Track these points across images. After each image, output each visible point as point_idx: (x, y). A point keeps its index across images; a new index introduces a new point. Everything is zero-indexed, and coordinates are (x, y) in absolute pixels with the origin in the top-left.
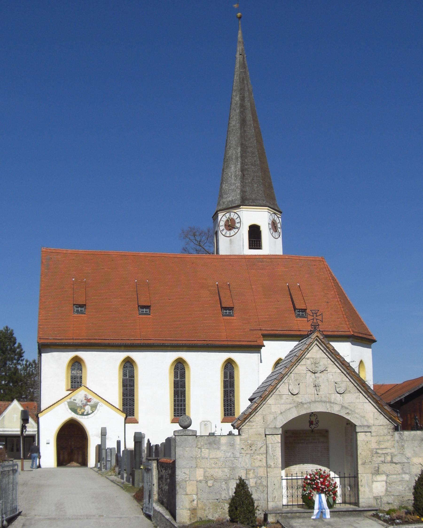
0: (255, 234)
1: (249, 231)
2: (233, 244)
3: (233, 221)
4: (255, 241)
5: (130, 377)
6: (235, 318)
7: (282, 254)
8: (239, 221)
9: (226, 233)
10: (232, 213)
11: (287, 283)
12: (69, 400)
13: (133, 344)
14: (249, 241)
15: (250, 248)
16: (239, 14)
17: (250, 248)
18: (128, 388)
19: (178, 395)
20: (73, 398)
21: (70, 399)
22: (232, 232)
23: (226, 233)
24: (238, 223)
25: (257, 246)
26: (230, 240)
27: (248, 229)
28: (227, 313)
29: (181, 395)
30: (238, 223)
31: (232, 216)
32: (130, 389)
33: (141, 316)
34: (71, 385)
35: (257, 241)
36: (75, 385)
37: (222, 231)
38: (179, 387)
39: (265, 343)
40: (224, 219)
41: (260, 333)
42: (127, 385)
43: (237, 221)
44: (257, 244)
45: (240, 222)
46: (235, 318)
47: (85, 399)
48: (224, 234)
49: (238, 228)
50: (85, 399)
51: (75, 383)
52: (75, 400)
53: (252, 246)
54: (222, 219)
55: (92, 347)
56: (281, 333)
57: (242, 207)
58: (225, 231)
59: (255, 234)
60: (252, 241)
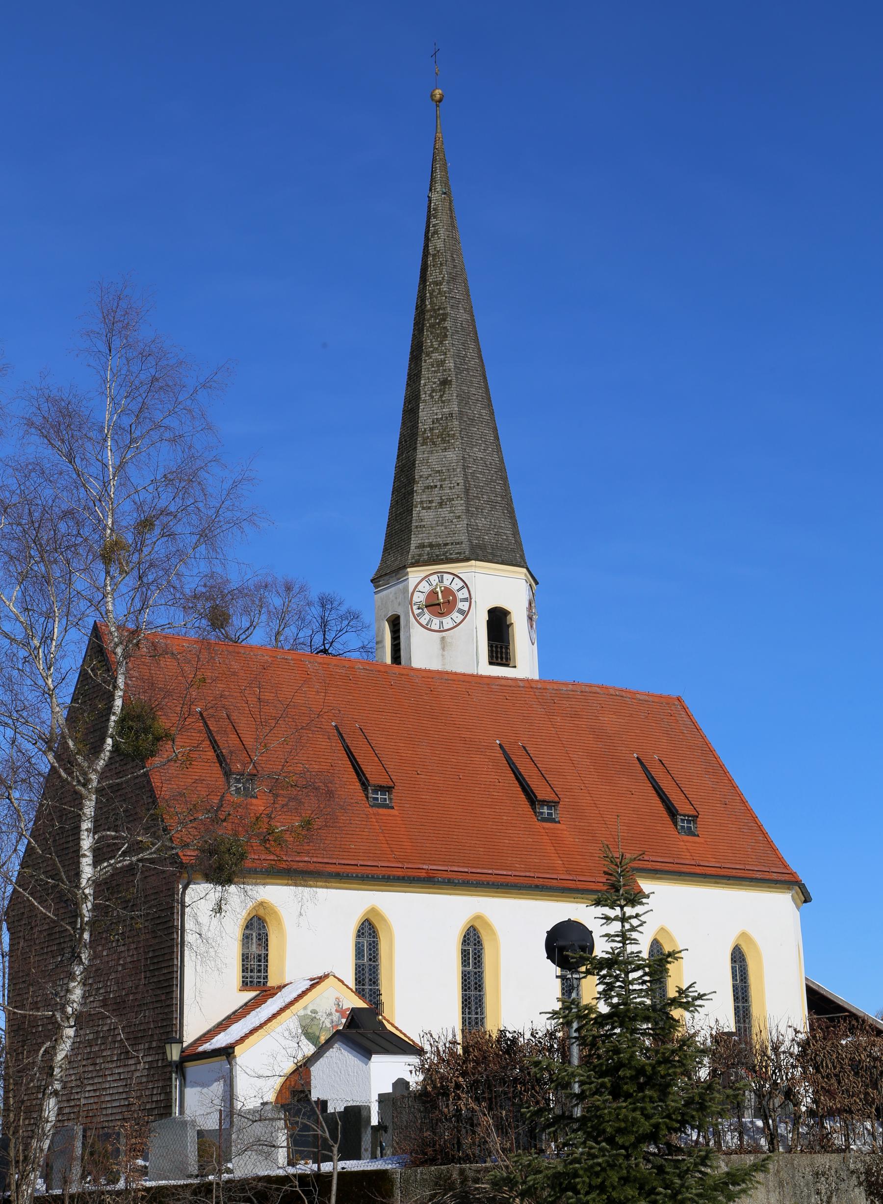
0: (498, 623)
1: (488, 621)
2: (448, 649)
3: (447, 591)
4: (497, 647)
5: (370, 960)
7: (537, 677)
8: (467, 595)
9: (430, 621)
10: (446, 576)
11: (633, 752)
12: (301, 1013)
14: (490, 646)
15: (491, 663)
16: (438, 92)
17: (491, 663)
18: (367, 987)
19: (469, 1008)
20: (310, 1008)
21: (305, 1008)
22: (447, 622)
23: (430, 621)
25: (502, 658)
26: (443, 638)
27: (486, 617)
28: (542, 813)
29: (477, 1008)
31: (446, 583)
32: (371, 990)
33: (375, 810)
34: (243, 977)
35: (501, 648)
36: (251, 977)
38: (473, 988)
40: (425, 587)
42: (363, 980)
43: (461, 595)
44: (502, 653)
45: (469, 599)
47: (337, 1011)
48: (424, 623)
50: (337, 1011)
51: (252, 971)
53: (497, 658)
54: (420, 588)
55: (744, 883)
57: (473, 562)
59: (498, 623)
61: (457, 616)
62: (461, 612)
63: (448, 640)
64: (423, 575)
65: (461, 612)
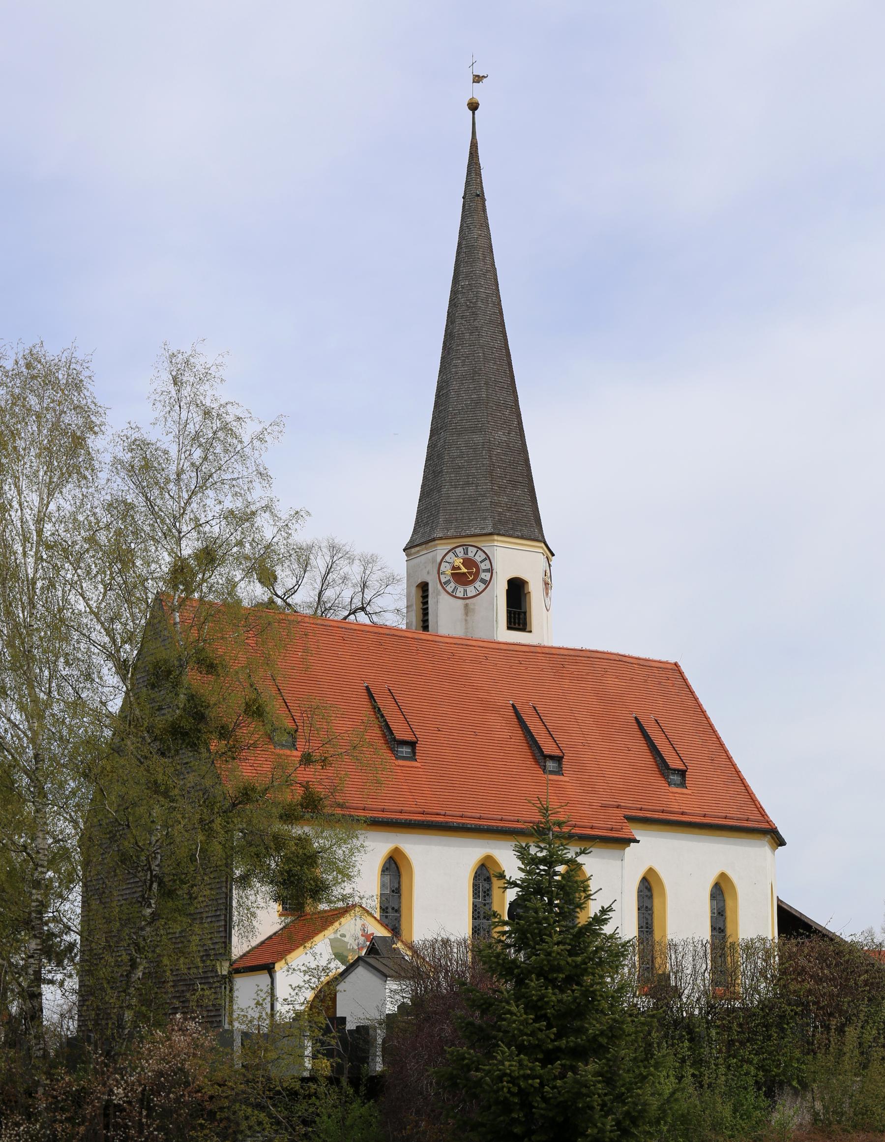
6: (689, 792)
9: (455, 589)
12: (332, 936)
13: (411, 820)
15: (509, 628)
17: (509, 628)
22: (471, 591)
23: (455, 589)
24: (484, 571)
25: (519, 625)
26: (466, 606)
27: (505, 586)
30: (484, 571)
37: (445, 583)
39: (637, 832)
41: (621, 813)
44: (519, 619)
45: (491, 570)
46: (689, 792)
47: (362, 935)
48: (450, 590)
49: (487, 583)
50: (362, 935)
52: (343, 936)
56: (656, 816)
57: (496, 537)
58: (453, 585)
60: (515, 613)
61: (480, 586)
62: (483, 581)
63: (471, 607)
64: (450, 547)
65: (483, 581)
